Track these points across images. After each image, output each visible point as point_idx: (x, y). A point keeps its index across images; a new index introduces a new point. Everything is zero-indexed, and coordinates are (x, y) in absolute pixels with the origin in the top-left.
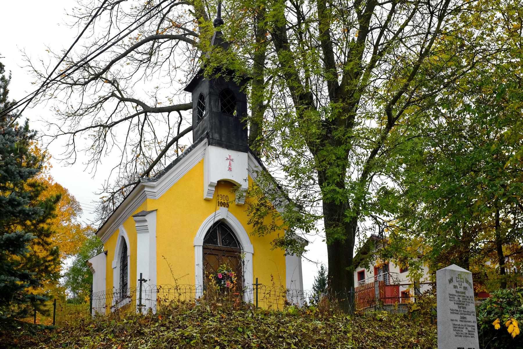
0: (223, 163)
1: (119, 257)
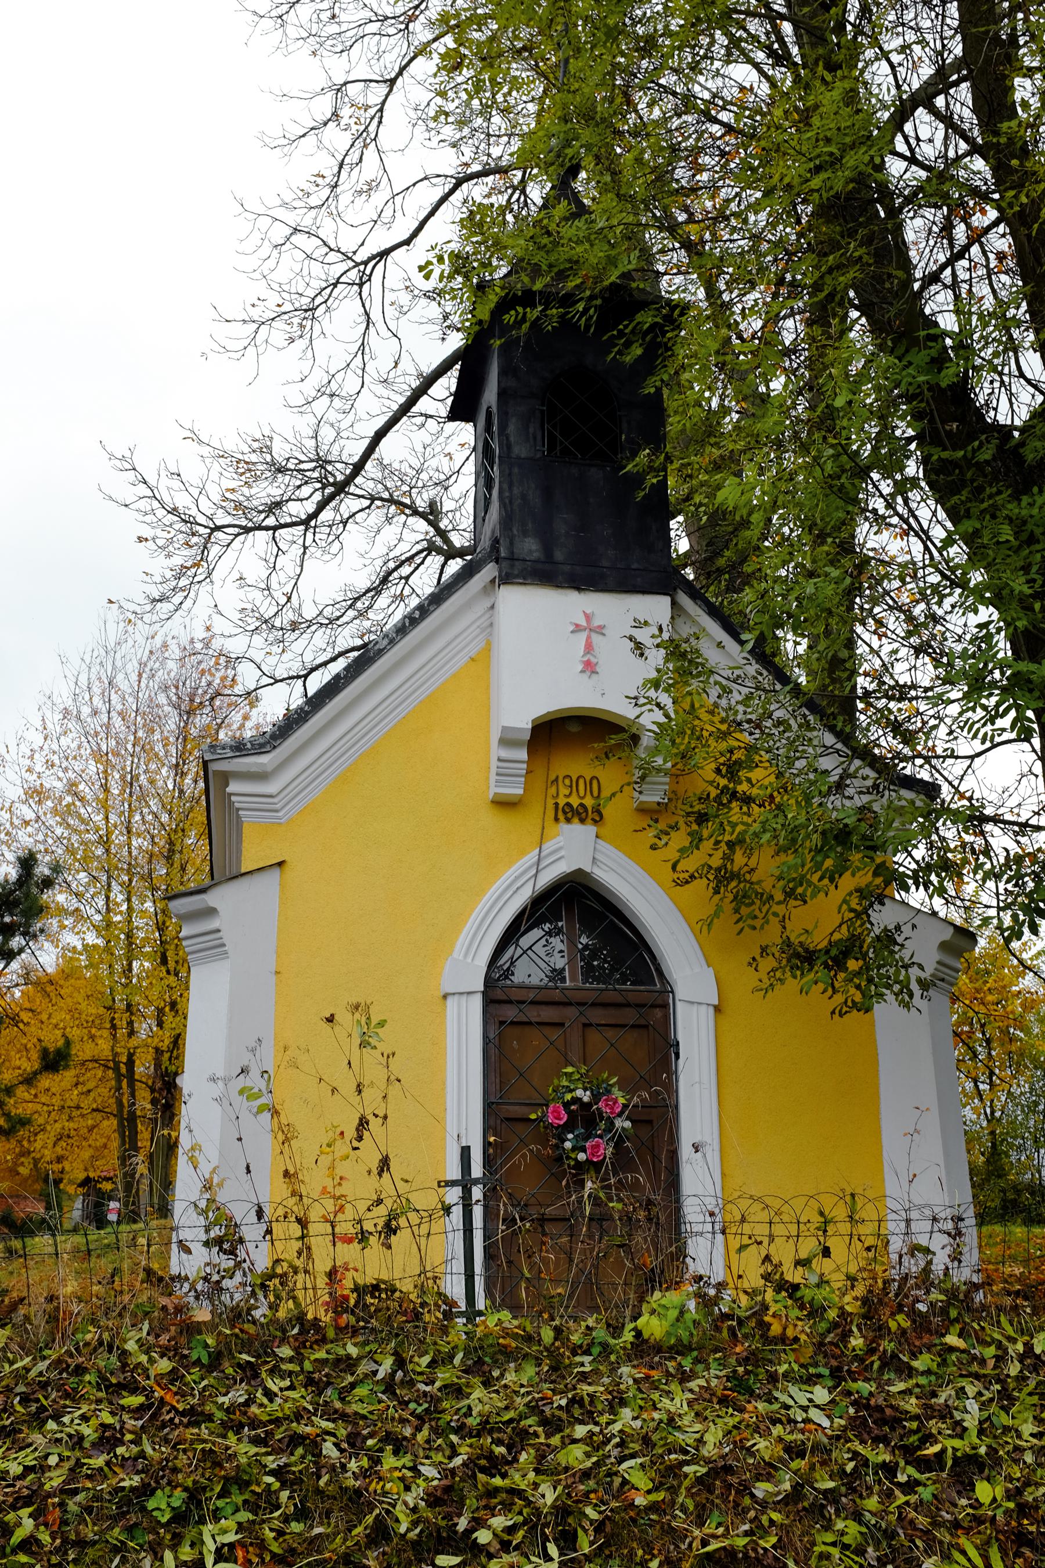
0: (570, 647)
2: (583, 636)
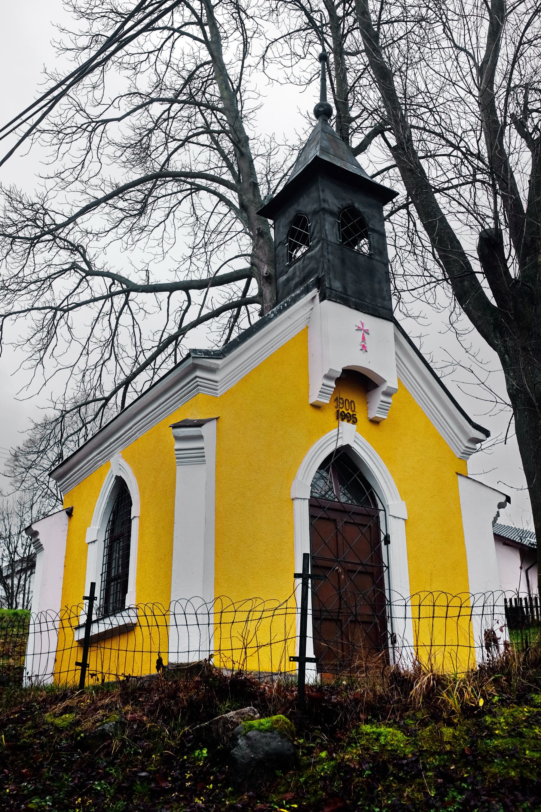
1: (103, 520)
2: (360, 333)
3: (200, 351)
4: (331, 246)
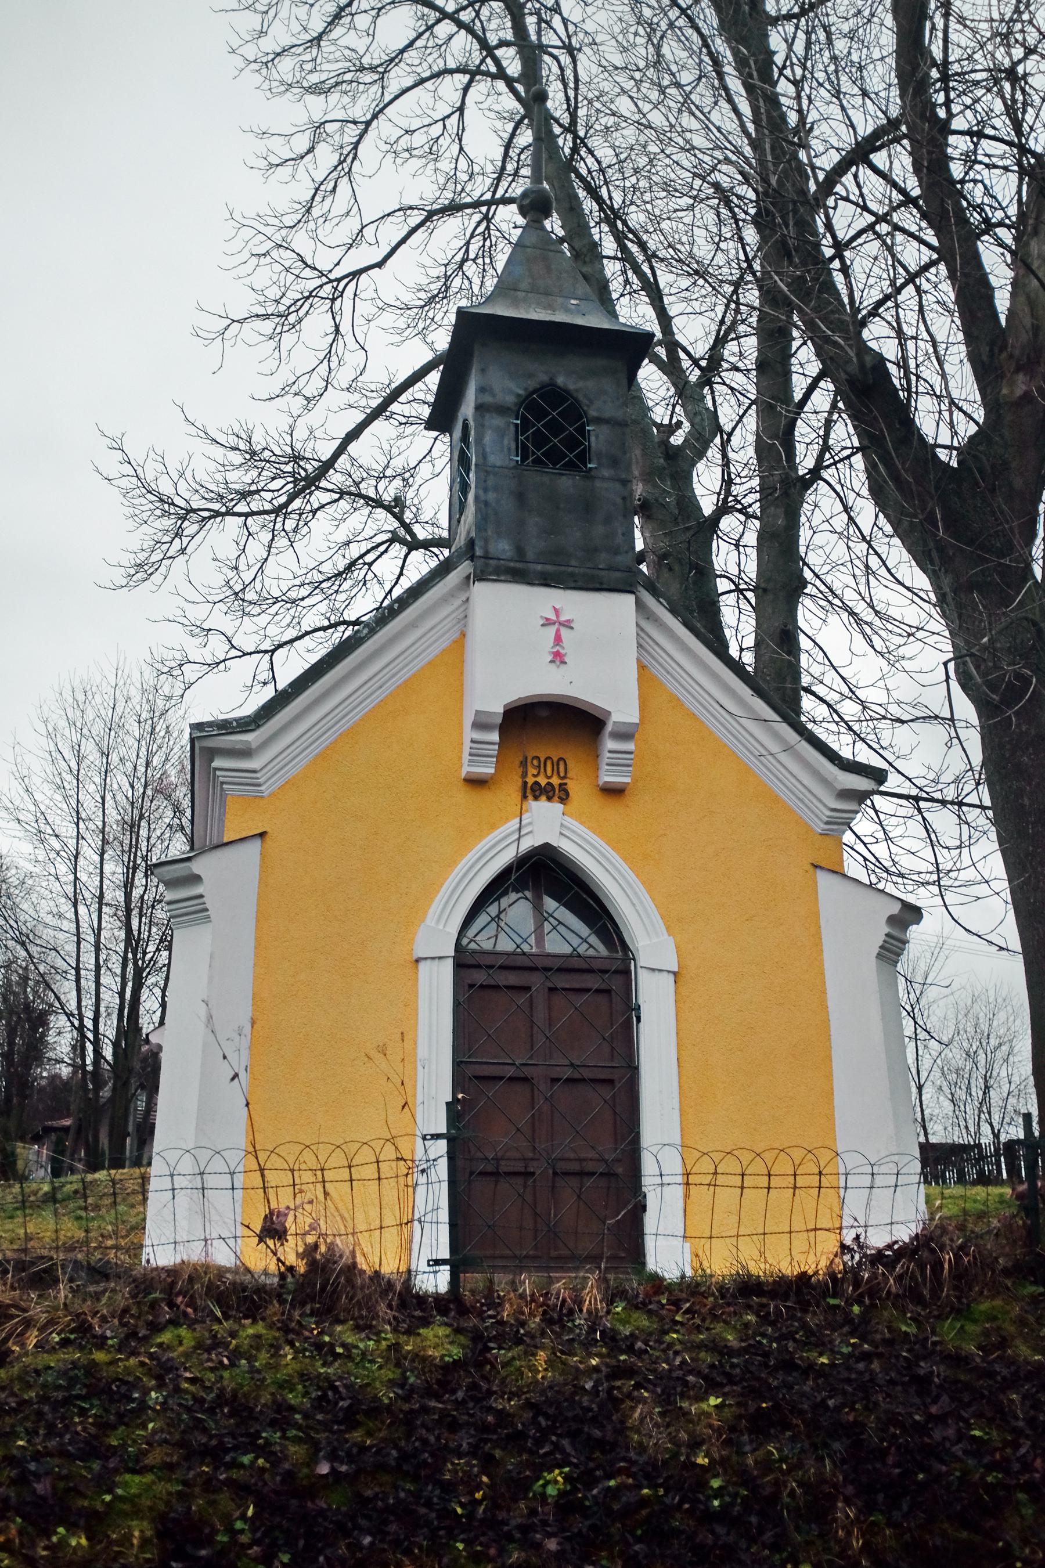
2: (552, 631)
3: (210, 724)
4: (495, 474)
